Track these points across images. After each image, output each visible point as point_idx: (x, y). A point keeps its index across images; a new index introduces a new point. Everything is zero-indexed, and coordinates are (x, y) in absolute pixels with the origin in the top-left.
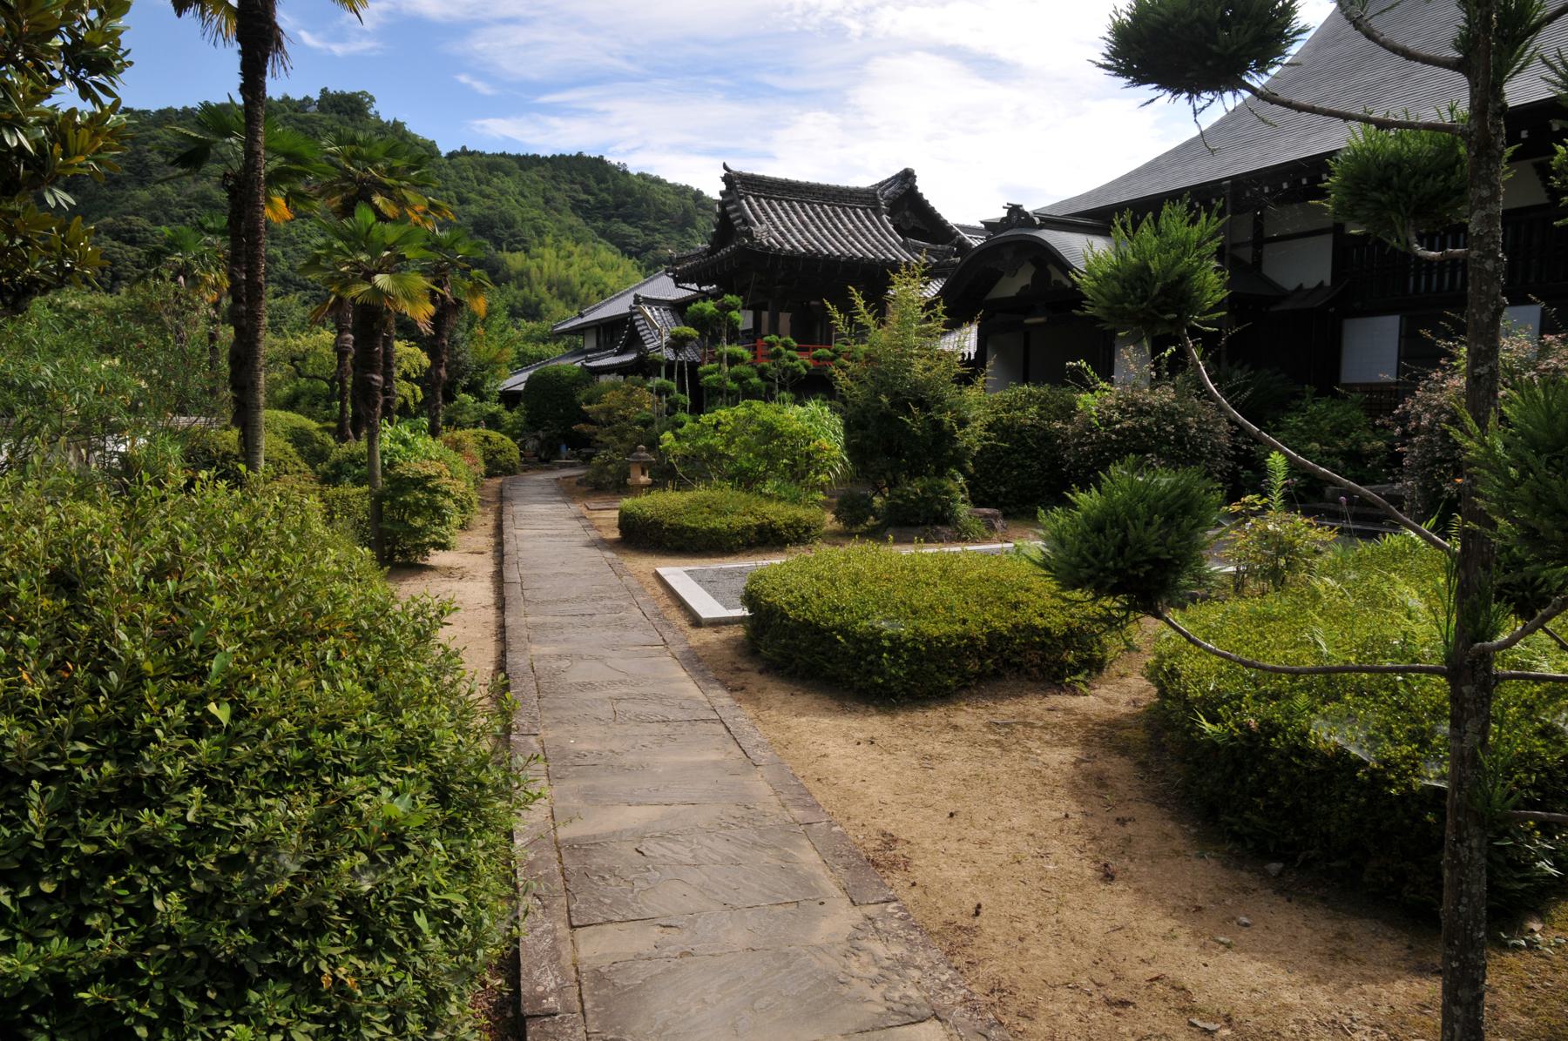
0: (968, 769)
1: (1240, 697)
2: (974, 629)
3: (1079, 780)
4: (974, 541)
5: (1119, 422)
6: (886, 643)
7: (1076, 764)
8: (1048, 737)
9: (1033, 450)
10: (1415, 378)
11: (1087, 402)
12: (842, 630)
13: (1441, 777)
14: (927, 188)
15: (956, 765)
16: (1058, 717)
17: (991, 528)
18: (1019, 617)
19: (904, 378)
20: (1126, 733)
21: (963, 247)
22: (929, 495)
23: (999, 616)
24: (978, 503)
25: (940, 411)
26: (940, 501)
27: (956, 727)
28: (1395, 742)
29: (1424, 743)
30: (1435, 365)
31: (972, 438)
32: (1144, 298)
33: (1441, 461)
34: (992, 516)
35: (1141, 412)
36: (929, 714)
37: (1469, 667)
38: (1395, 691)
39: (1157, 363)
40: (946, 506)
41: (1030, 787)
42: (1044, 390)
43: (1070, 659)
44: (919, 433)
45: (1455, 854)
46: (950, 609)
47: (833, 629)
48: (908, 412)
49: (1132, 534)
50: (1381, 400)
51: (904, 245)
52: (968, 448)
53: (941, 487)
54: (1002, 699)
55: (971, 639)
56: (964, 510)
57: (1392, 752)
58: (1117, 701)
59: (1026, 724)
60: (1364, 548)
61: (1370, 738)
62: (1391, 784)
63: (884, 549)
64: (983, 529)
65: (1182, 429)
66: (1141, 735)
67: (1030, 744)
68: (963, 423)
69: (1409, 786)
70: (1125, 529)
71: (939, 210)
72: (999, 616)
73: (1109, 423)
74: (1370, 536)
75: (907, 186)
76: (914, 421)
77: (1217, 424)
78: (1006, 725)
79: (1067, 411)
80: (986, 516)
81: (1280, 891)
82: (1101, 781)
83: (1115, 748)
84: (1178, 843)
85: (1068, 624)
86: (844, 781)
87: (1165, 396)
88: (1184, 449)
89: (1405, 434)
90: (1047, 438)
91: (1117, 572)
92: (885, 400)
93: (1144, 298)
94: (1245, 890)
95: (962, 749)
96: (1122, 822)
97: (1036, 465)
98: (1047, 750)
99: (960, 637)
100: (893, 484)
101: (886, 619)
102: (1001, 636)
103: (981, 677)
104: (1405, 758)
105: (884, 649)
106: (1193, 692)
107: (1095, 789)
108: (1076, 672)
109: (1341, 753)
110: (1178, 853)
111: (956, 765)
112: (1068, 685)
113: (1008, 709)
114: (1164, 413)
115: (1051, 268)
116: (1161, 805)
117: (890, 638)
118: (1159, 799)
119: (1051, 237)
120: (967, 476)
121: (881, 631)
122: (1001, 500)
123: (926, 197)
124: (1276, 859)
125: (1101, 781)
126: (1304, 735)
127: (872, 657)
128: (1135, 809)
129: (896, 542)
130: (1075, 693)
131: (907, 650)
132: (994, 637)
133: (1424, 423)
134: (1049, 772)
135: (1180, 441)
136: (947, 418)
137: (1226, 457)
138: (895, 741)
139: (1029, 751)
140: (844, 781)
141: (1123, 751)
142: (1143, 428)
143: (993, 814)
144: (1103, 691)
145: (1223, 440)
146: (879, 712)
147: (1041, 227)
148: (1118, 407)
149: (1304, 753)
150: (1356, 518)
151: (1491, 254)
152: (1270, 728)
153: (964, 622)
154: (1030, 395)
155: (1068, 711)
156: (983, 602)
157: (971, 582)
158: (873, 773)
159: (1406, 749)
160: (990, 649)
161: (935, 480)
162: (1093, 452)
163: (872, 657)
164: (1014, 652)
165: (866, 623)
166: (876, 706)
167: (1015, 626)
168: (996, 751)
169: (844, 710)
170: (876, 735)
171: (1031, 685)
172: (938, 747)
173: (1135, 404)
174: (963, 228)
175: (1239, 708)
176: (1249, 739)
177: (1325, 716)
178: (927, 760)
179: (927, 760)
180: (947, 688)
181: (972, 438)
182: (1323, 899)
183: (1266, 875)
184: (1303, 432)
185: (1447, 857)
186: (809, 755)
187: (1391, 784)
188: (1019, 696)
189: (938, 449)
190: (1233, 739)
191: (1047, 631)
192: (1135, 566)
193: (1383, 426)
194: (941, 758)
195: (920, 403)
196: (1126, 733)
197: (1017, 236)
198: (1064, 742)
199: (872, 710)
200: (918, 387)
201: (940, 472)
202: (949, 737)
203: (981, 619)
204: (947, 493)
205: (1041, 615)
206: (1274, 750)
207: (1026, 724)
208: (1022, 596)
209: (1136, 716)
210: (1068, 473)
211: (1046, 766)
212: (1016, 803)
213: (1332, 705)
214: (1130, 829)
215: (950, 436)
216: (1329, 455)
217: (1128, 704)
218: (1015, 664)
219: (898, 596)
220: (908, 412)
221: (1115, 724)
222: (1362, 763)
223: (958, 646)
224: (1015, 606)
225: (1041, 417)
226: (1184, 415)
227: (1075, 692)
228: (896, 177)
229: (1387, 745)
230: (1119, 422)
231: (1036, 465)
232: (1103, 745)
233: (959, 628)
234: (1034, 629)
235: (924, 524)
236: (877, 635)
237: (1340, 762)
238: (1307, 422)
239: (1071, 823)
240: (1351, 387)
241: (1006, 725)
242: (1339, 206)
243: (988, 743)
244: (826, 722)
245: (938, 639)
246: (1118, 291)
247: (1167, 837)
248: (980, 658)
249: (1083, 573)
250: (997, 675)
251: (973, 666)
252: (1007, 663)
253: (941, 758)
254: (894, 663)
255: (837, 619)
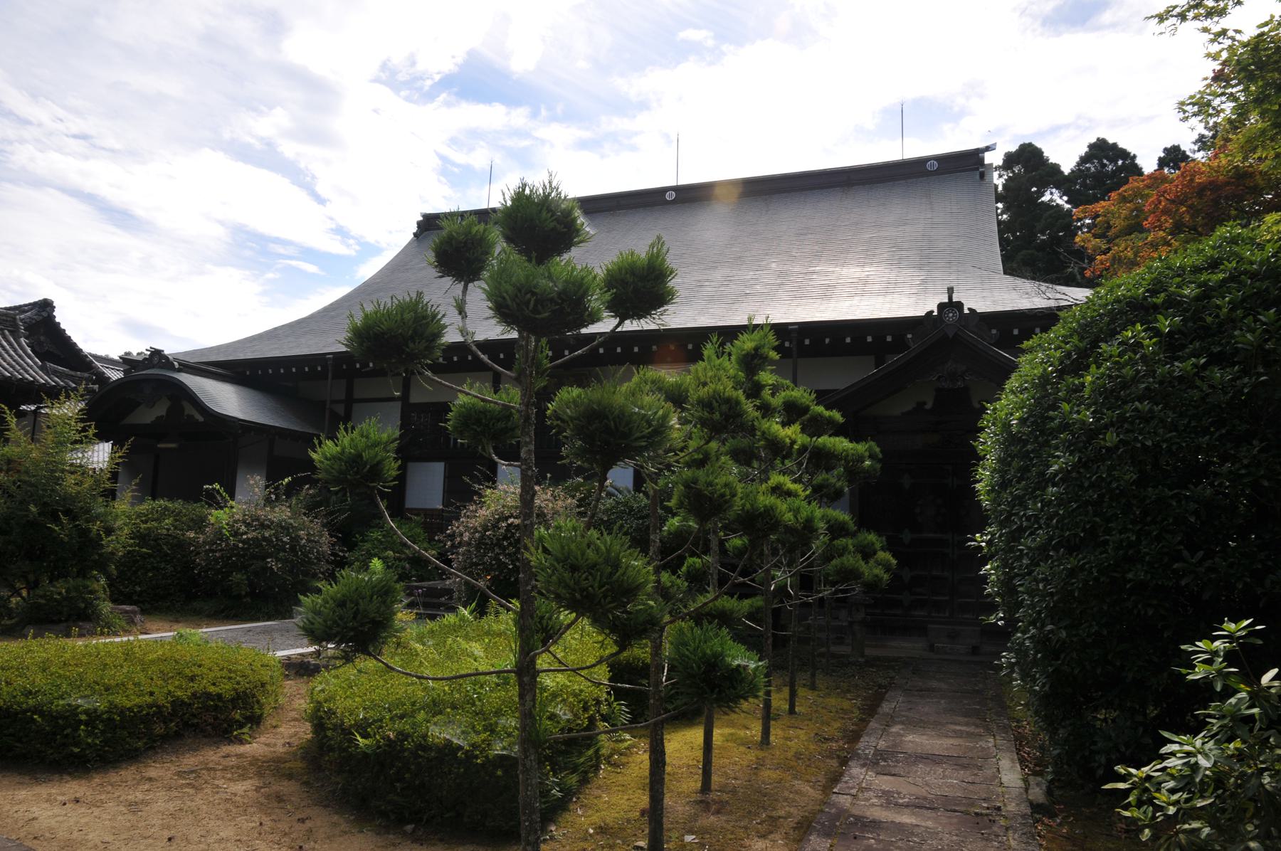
0: (171, 806)
1: (381, 720)
2: (161, 700)
3: (262, 800)
4: (116, 634)
5: (243, 534)
6: (83, 717)
7: (258, 789)
8: (229, 776)
9: (167, 555)
10: (458, 508)
11: (219, 517)
12: (36, 710)
13: (504, 748)
14: (66, 318)
15: (161, 805)
16: (233, 761)
17: (131, 622)
18: (196, 686)
19: (52, 490)
20: (288, 765)
21: (102, 379)
22: (73, 594)
23: (180, 687)
24: (114, 601)
25: (88, 521)
26: (84, 600)
27: (150, 779)
28: (478, 733)
29: (492, 731)
30: (471, 500)
31: (118, 544)
32: (357, 473)
33: (477, 564)
34: (134, 612)
35: (263, 526)
36: (122, 773)
37: (526, 672)
38: (474, 704)
39: (277, 488)
40: (89, 604)
41: (227, 811)
42: (177, 505)
43: (237, 717)
44: (66, 539)
45: (524, 765)
46: (137, 684)
47: (29, 710)
48: (56, 520)
49: (362, 607)
50: (435, 523)
51: (41, 368)
52: (112, 553)
53: (86, 587)
54: (183, 754)
55: (158, 707)
56: (106, 607)
57: (477, 739)
58: (275, 745)
59: (209, 769)
60: (430, 625)
61: (463, 732)
62: (477, 757)
63: (69, 642)
64: (124, 623)
65: (295, 540)
66: (300, 765)
67: (216, 782)
68: (109, 531)
69: (487, 757)
70: (357, 604)
71: (75, 339)
72: (180, 687)
73: (236, 534)
74: (433, 617)
75: (45, 314)
76: (62, 529)
77: (321, 536)
78: (192, 772)
79: (199, 523)
80: (127, 612)
81: (415, 841)
82: (279, 799)
83: (283, 775)
84: (344, 826)
85: (235, 690)
86: (62, 834)
87: (281, 513)
88: (296, 555)
89: (453, 546)
90: (180, 545)
91: (353, 629)
92: (33, 508)
93: (357, 473)
94: (394, 845)
95: (161, 794)
96: (302, 821)
97: (170, 568)
98: (232, 784)
99: (150, 706)
100: (33, 586)
101: (81, 697)
102: (183, 703)
103: (165, 738)
104: (483, 741)
105: (81, 722)
106: (348, 721)
107: (276, 804)
108: (241, 726)
109: (449, 743)
110: (346, 833)
111: (161, 805)
112: (236, 737)
113: (190, 761)
114: (282, 527)
115: (185, 404)
116: (325, 806)
117: (86, 712)
118: (324, 803)
119: (188, 379)
120: (109, 577)
121: (79, 706)
122: (135, 598)
123: (62, 326)
124: (408, 823)
125: (279, 799)
126: (425, 736)
127: (68, 731)
128: (308, 812)
129: (81, 635)
130: (242, 742)
131: (102, 721)
132: (178, 704)
133: (466, 539)
134: (238, 798)
135: (293, 549)
136: (96, 527)
137: (327, 561)
138: (98, 797)
139: (218, 786)
140: (62, 834)
141: (290, 776)
142: (264, 539)
143: (203, 833)
144: (262, 739)
145: (325, 548)
146: (74, 778)
147: (179, 370)
148: (244, 522)
149: (425, 747)
150: (426, 606)
151: (530, 468)
152: (403, 736)
153: (152, 694)
154: (166, 508)
155: (239, 756)
156: (164, 677)
157: (152, 662)
158: (87, 824)
159: (483, 736)
160: (174, 714)
161: (79, 581)
162: (222, 557)
163: (68, 731)
164: (194, 716)
165: (61, 702)
166: (70, 774)
167: (194, 694)
168: (192, 791)
169: (37, 781)
170: (78, 795)
171: (205, 740)
172: (140, 796)
173: (258, 520)
174: (95, 357)
175: (381, 727)
176: (389, 746)
177: (435, 724)
178: (134, 807)
179: (134, 807)
180: (136, 750)
181: (118, 544)
182: (441, 840)
183: (405, 834)
184: (381, 543)
185: (520, 768)
186: (16, 822)
187: (477, 757)
188: (196, 750)
189: (84, 553)
190: (379, 747)
191: (219, 696)
192: (362, 625)
193: (439, 541)
194: (145, 803)
195: (67, 512)
196: (288, 765)
197: (153, 377)
198: (243, 777)
199: (66, 777)
200: (66, 498)
201: (83, 573)
202: (146, 787)
203: (163, 691)
204: (91, 592)
205: (214, 684)
206: (405, 750)
207: (209, 769)
208: (196, 671)
209: (295, 754)
210: (199, 573)
211: (235, 795)
212: (219, 823)
213: (439, 717)
214: (309, 824)
215: (96, 543)
216: (400, 560)
217: (284, 745)
218: (193, 725)
219: (91, 677)
220: (56, 520)
221: (278, 760)
222: (460, 748)
223: (148, 714)
224: (192, 679)
225: (176, 528)
226: (296, 529)
227: (242, 742)
228: (34, 304)
229: (473, 735)
230: (246, 533)
231: (170, 568)
232: (274, 775)
233: (148, 699)
234: (208, 695)
235: (66, 621)
236: (74, 710)
237: (449, 749)
238: (384, 536)
239: (265, 828)
240: (417, 512)
241: (192, 772)
242: (455, 427)
243: (182, 786)
244: (22, 794)
245: (130, 709)
246: (344, 467)
247: (335, 825)
248: (165, 723)
249: (335, 630)
250: (178, 735)
251: (159, 729)
252: (187, 725)
253: (145, 803)
254: (89, 734)
255: (30, 702)
